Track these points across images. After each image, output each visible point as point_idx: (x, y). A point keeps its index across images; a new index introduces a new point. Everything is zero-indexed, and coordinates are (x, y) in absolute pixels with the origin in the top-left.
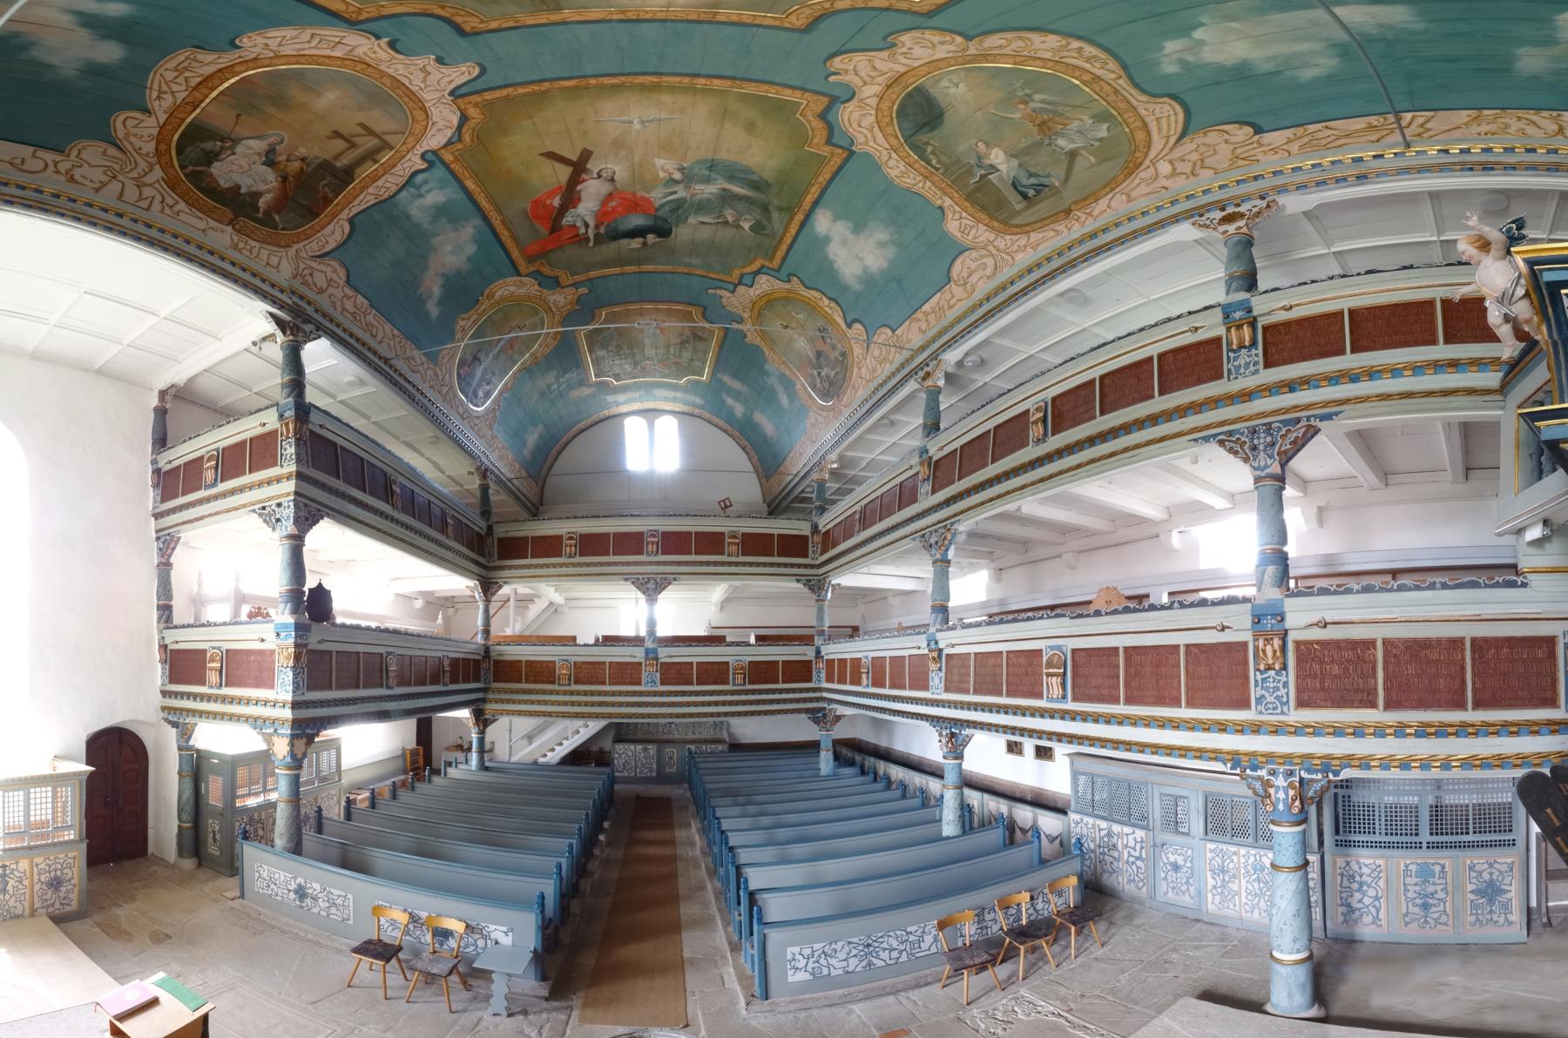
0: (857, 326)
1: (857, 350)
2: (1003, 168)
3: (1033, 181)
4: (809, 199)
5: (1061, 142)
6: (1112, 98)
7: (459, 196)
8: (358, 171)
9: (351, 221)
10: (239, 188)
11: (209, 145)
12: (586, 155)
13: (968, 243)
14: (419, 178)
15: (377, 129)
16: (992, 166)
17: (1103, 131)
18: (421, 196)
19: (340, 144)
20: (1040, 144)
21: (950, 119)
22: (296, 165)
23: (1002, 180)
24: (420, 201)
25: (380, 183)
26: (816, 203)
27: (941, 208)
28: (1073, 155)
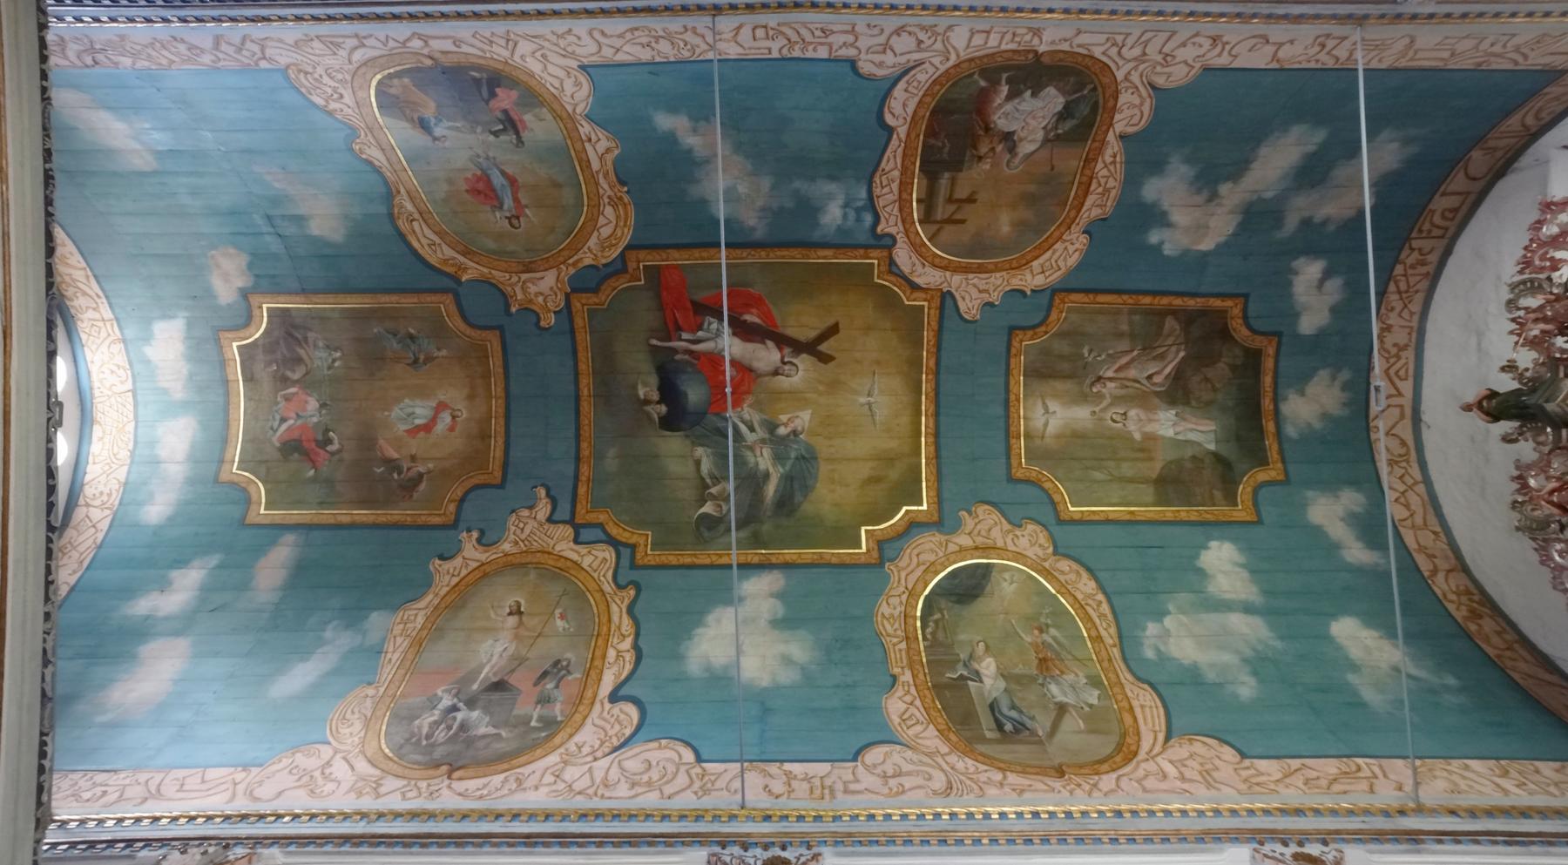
0: (633, 711)
1: (587, 736)
2: (988, 682)
3: (1013, 714)
4: (790, 554)
5: (1054, 688)
6: (1106, 664)
7: (816, 236)
8: (925, 182)
9: (890, 130)
10: (1034, 95)
11: (1069, 124)
12: (825, 359)
13: (905, 739)
14: (868, 218)
15: (949, 228)
16: (977, 673)
17: (1093, 697)
18: (846, 206)
19: (962, 192)
20: (1033, 679)
21: (981, 605)
22: (983, 150)
23: (981, 694)
24: (840, 202)
25: (895, 186)
26: (786, 566)
27: (895, 678)
28: (1062, 709)
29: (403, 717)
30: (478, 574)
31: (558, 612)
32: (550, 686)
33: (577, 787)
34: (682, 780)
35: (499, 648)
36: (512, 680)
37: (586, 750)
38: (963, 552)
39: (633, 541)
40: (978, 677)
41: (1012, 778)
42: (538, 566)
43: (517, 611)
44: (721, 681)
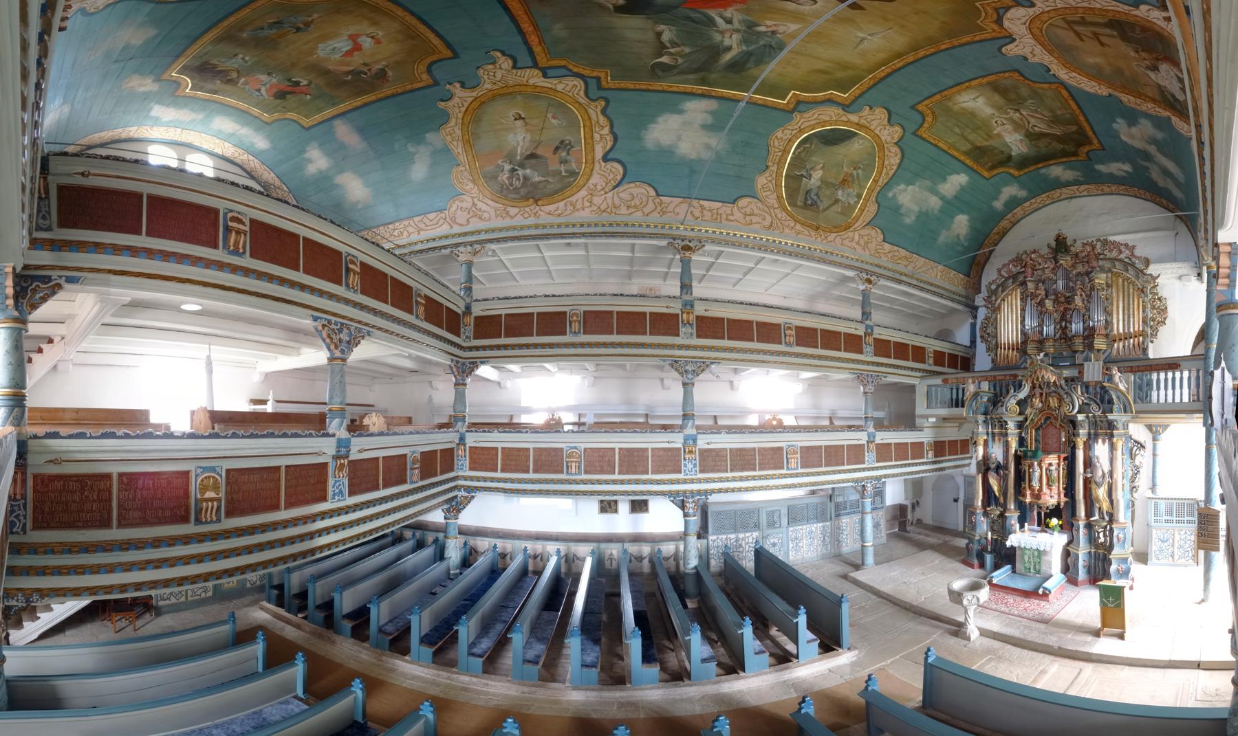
2: (813, 180)
13: (760, 196)
28: (837, 201)
29: (491, 178)
30: (477, 103)
31: (549, 115)
32: (564, 154)
33: (603, 207)
34: (651, 206)
35: (520, 138)
36: (539, 152)
37: (599, 188)
38: (848, 122)
39: (595, 74)
40: (810, 177)
41: (798, 227)
42: (520, 93)
43: (519, 117)
44: (666, 154)
